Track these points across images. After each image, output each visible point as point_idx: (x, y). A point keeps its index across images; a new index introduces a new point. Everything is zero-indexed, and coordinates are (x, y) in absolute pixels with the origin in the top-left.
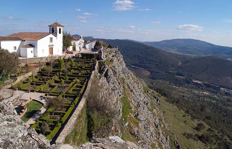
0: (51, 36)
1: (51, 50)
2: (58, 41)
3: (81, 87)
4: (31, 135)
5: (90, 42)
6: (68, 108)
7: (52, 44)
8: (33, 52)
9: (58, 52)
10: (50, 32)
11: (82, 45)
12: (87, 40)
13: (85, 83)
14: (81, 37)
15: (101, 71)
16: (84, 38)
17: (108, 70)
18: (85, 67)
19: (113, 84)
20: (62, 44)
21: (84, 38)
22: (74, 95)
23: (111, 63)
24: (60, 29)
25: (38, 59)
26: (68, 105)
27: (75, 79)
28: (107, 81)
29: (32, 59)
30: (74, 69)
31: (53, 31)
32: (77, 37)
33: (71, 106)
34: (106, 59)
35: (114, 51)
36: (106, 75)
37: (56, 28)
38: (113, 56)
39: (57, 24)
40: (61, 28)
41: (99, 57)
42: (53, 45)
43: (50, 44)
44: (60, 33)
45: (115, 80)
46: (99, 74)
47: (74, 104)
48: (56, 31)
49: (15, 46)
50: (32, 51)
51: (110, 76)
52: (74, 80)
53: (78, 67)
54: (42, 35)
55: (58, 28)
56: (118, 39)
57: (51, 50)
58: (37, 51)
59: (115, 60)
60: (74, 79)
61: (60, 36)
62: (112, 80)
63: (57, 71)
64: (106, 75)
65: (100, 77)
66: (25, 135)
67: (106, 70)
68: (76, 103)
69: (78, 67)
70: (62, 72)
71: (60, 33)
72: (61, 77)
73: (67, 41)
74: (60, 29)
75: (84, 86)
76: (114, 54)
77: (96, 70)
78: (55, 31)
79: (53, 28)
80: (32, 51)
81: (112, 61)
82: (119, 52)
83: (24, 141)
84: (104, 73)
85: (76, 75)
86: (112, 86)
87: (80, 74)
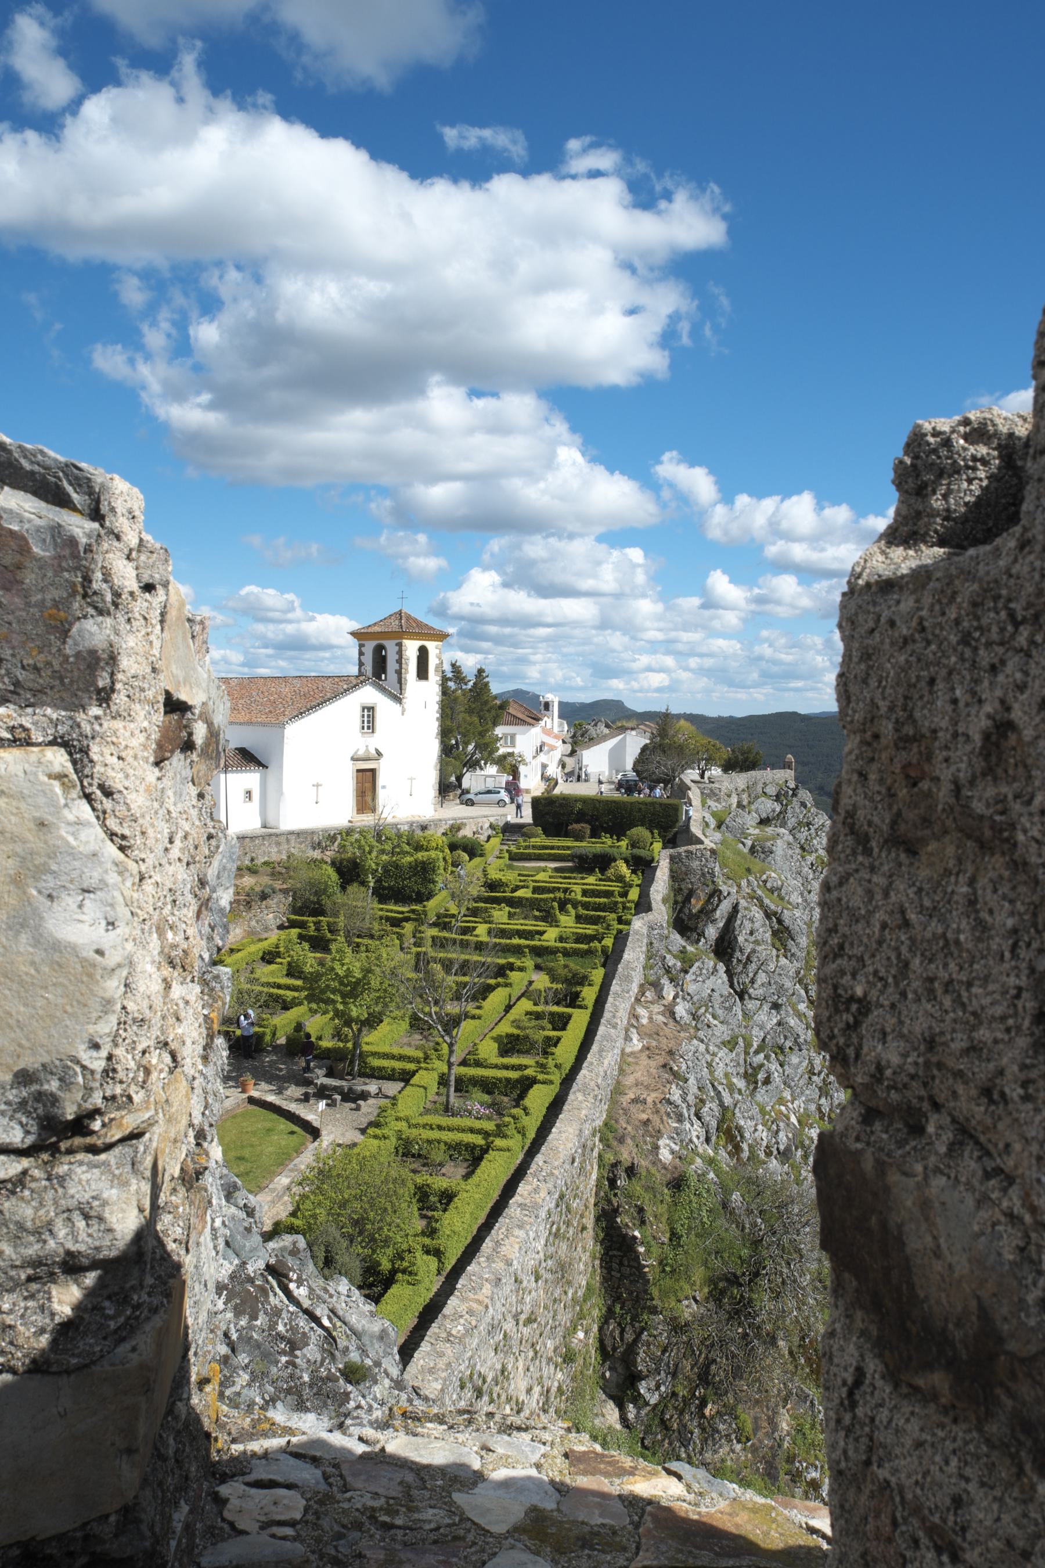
0: (368, 694)
1: (367, 783)
2: (410, 730)
3: (561, 1022)
4: (286, 1276)
5: (606, 731)
6: (475, 1157)
7: (372, 743)
8: (256, 795)
9: (411, 797)
10: (361, 673)
11: (557, 755)
12: (586, 722)
13: (589, 994)
14: (547, 706)
15: (685, 924)
16: (568, 712)
17: (735, 909)
18: (585, 893)
19: (776, 1006)
20: (434, 747)
21: (568, 712)
22: (514, 1075)
23: (756, 865)
24: (423, 653)
25: (288, 840)
26: (479, 1140)
27: (521, 969)
28: (732, 986)
29: (252, 838)
30: (511, 902)
31: (379, 667)
32: (532, 710)
33: (499, 1142)
34: (718, 836)
35: (772, 790)
36: (725, 948)
37: (400, 645)
38: (764, 822)
39: (405, 626)
40: (432, 646)
41: (669, 825)
42: (379, 753)
43: (364, 744)
44: (422, 673)
45: (788, 984)
46: (677, 940)
47: (522, 1132)
48: (399, 661)
49: (423, 683)
50: (249, 794)
51: (754, 951)
52: (514, 976)
53: (536, 890)
54: (316, 694)
55: (411, 648)
56: (795, 714)
57: (367, 783)
58: (280, 792)
59: (780, 847)
60: (511, 967)
61: (424, 698)
62: (762, 978)
63: (407, 919)
64: (725, 948)
65: (687, 962)
66: (250, 1269)
67: (725, 907)
68: (532, 1124)
69: (536, 890)
70: (435, 925)
71: (422, 673)
72: (432, 953)
73: (473, 719)
74: (423, 653)
75: (580, 1019)
76: (768, 806)
77: (661, 912)
78: (391, 665)
79: (379, 649)
80: (249, 794)
81: (760, 851)
82: (805, 795)
83: (238, 1312)
84: (712, 932)
85: (510, 948)
86: (767, 1019)
87: (551, 935)
